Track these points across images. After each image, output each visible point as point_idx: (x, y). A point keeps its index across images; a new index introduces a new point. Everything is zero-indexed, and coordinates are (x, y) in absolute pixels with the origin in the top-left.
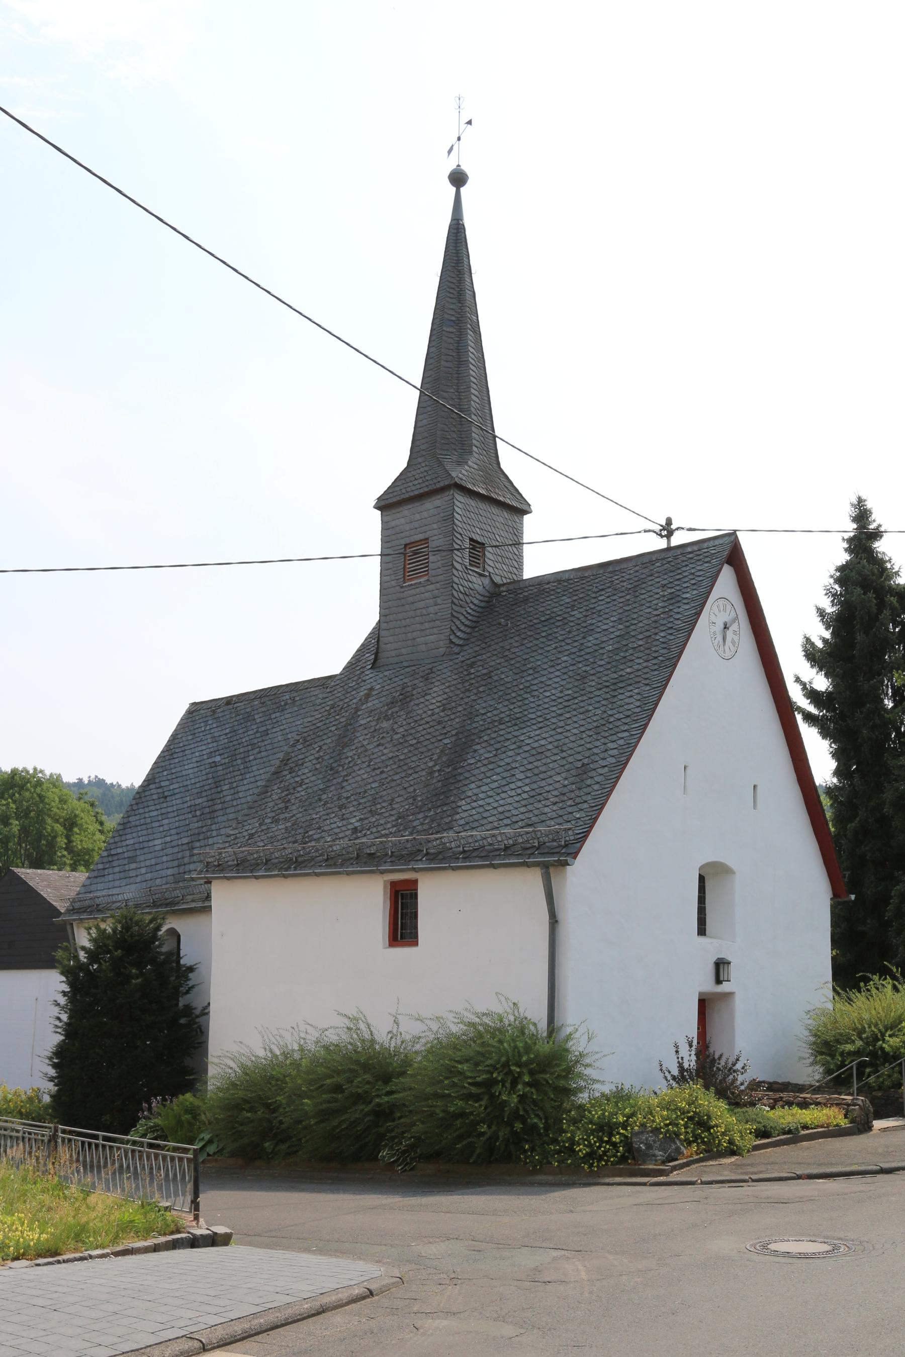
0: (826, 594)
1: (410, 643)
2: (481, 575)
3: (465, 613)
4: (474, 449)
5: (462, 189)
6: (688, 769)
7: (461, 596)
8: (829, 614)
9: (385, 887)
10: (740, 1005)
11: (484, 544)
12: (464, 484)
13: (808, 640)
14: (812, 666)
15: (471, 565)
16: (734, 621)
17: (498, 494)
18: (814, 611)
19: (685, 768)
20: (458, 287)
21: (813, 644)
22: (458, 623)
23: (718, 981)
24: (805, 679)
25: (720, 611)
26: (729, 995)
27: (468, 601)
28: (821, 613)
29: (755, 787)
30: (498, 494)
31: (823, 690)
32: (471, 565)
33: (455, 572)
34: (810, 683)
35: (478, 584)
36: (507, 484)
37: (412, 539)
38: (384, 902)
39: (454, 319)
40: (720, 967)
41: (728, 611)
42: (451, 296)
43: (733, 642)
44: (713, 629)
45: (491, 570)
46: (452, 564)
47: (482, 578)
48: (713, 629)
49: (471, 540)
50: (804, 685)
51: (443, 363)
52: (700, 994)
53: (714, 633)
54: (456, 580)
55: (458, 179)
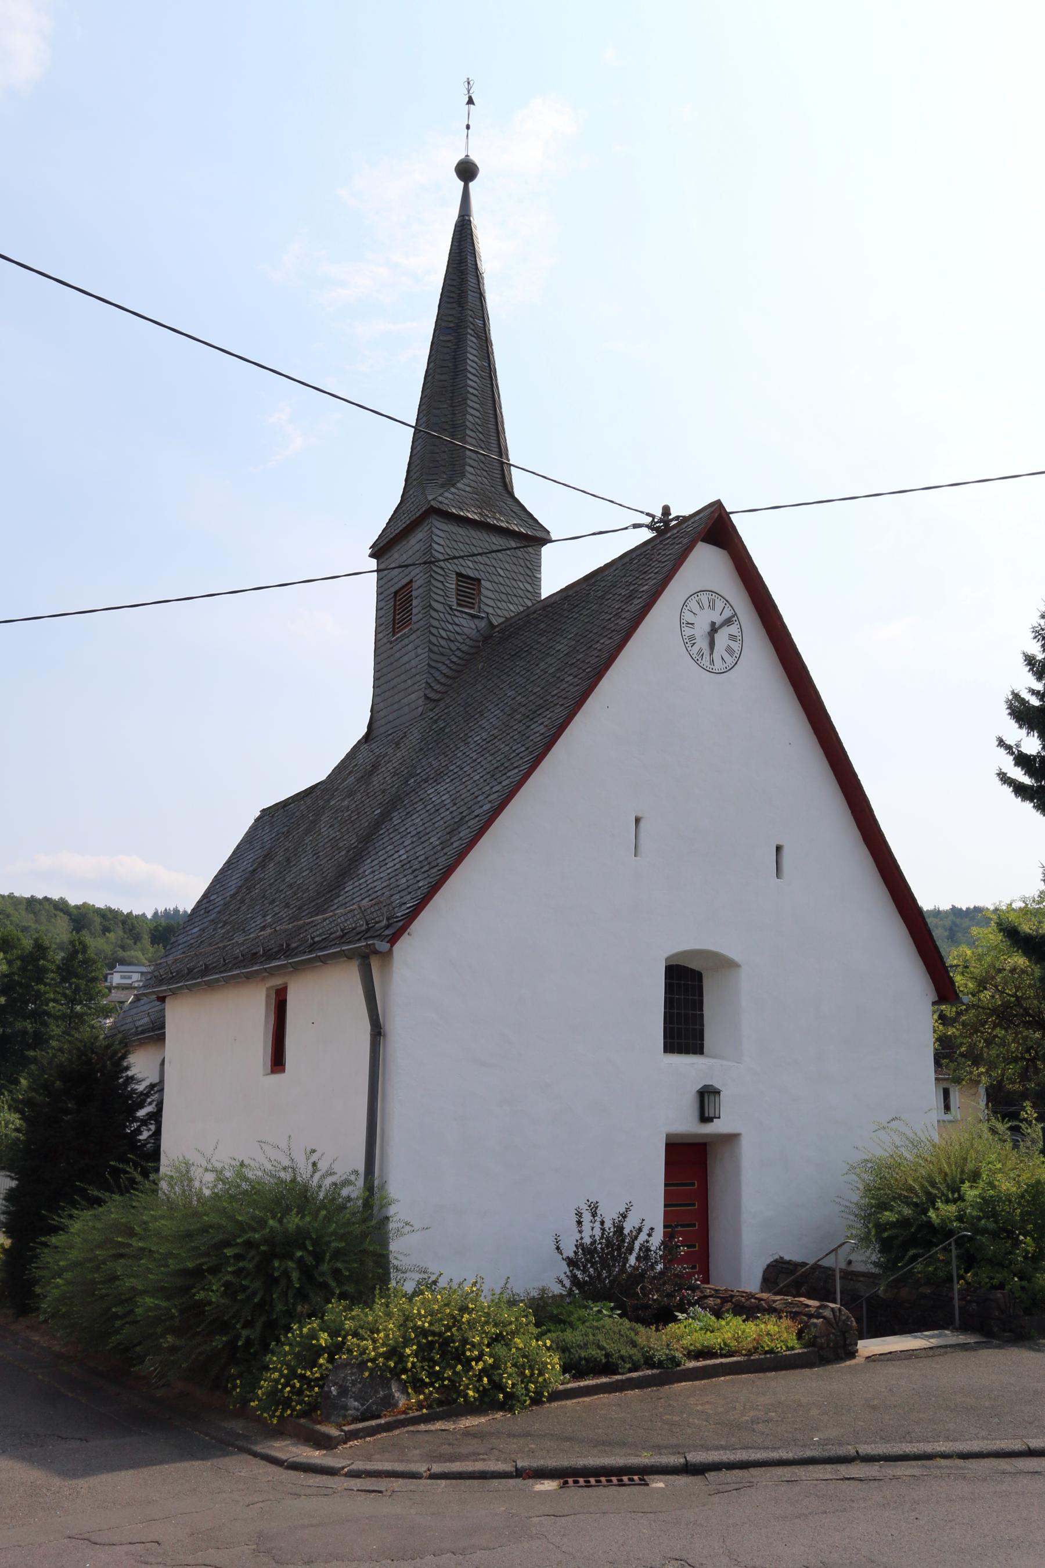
0: (1035, 638)
1: (395, 707)
2: (473, 616)
3: (447, 662)
4: (468, 468)
5: (471, 185)
6: (642, 824)
7: (443, 642)
8: (1040, 661)
9: (268, 996)
10: (749, 1152)
11: (479, 580)
12: (444, 508)
13: (1016, 696)
14: (1021, 727)
15: (459, 605)
16: (728, 622)
17: (498, 520)
18: (1021, 659)
19: (637, 820)
20: (459, 289)
21: (1023, 701)
22: (436, 674)
23: (705, 1118)
24: (1010, 741)
25: (702, 608)
26: (731, 1139)
27: (454, 648)
28: (1030, 661)
29: (779, 849)
30: (498, 520)
31: (1034, 753)
32: (459, 605)
33: (434, 614)
34: (1018, 746)
35: (469, 627)
36: (516, 509)
37: (400, 585)
38: (266, 1017)
39: (452, 325)
40: (707, 1098)
41: (718, 609)
42: (452, 300)
43: (730, 650)
44: (688, 631)
45: (490, 610)
46: (430, 605)
47: (477, 621)
48: (688, 631)
49: (459, 575)
50: (1009, 748)
51: (438, 377)
52: (668, 1136)
53: (692, 638)
54: (435, 623)
55: (467, 171)
